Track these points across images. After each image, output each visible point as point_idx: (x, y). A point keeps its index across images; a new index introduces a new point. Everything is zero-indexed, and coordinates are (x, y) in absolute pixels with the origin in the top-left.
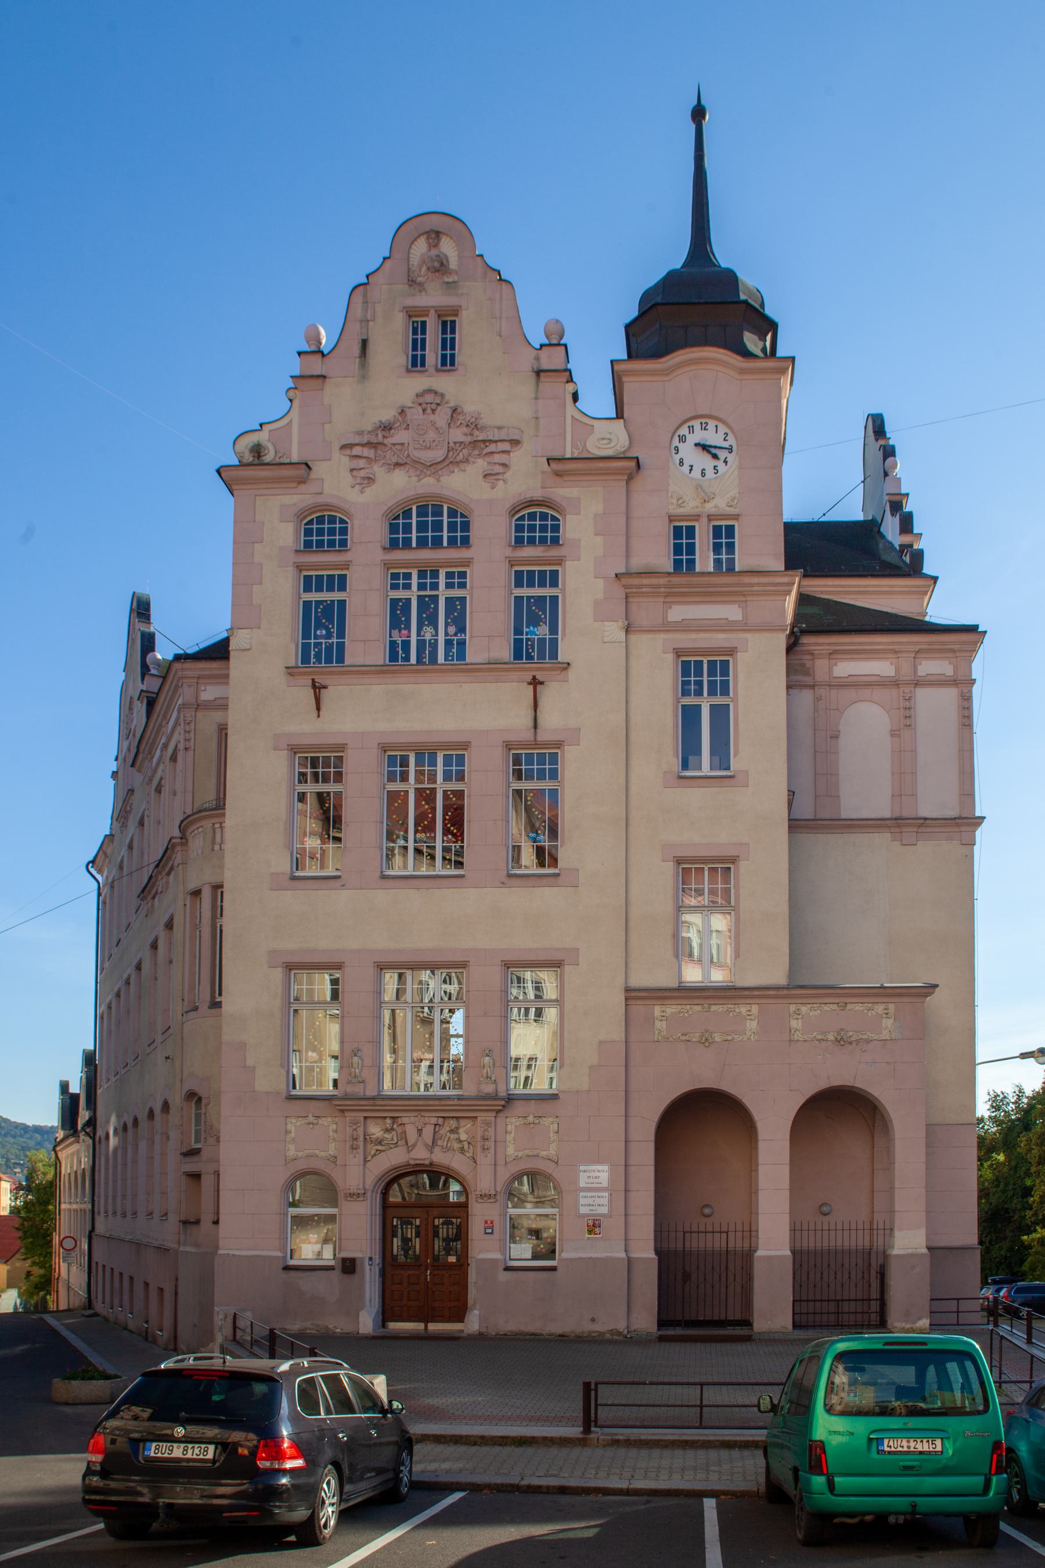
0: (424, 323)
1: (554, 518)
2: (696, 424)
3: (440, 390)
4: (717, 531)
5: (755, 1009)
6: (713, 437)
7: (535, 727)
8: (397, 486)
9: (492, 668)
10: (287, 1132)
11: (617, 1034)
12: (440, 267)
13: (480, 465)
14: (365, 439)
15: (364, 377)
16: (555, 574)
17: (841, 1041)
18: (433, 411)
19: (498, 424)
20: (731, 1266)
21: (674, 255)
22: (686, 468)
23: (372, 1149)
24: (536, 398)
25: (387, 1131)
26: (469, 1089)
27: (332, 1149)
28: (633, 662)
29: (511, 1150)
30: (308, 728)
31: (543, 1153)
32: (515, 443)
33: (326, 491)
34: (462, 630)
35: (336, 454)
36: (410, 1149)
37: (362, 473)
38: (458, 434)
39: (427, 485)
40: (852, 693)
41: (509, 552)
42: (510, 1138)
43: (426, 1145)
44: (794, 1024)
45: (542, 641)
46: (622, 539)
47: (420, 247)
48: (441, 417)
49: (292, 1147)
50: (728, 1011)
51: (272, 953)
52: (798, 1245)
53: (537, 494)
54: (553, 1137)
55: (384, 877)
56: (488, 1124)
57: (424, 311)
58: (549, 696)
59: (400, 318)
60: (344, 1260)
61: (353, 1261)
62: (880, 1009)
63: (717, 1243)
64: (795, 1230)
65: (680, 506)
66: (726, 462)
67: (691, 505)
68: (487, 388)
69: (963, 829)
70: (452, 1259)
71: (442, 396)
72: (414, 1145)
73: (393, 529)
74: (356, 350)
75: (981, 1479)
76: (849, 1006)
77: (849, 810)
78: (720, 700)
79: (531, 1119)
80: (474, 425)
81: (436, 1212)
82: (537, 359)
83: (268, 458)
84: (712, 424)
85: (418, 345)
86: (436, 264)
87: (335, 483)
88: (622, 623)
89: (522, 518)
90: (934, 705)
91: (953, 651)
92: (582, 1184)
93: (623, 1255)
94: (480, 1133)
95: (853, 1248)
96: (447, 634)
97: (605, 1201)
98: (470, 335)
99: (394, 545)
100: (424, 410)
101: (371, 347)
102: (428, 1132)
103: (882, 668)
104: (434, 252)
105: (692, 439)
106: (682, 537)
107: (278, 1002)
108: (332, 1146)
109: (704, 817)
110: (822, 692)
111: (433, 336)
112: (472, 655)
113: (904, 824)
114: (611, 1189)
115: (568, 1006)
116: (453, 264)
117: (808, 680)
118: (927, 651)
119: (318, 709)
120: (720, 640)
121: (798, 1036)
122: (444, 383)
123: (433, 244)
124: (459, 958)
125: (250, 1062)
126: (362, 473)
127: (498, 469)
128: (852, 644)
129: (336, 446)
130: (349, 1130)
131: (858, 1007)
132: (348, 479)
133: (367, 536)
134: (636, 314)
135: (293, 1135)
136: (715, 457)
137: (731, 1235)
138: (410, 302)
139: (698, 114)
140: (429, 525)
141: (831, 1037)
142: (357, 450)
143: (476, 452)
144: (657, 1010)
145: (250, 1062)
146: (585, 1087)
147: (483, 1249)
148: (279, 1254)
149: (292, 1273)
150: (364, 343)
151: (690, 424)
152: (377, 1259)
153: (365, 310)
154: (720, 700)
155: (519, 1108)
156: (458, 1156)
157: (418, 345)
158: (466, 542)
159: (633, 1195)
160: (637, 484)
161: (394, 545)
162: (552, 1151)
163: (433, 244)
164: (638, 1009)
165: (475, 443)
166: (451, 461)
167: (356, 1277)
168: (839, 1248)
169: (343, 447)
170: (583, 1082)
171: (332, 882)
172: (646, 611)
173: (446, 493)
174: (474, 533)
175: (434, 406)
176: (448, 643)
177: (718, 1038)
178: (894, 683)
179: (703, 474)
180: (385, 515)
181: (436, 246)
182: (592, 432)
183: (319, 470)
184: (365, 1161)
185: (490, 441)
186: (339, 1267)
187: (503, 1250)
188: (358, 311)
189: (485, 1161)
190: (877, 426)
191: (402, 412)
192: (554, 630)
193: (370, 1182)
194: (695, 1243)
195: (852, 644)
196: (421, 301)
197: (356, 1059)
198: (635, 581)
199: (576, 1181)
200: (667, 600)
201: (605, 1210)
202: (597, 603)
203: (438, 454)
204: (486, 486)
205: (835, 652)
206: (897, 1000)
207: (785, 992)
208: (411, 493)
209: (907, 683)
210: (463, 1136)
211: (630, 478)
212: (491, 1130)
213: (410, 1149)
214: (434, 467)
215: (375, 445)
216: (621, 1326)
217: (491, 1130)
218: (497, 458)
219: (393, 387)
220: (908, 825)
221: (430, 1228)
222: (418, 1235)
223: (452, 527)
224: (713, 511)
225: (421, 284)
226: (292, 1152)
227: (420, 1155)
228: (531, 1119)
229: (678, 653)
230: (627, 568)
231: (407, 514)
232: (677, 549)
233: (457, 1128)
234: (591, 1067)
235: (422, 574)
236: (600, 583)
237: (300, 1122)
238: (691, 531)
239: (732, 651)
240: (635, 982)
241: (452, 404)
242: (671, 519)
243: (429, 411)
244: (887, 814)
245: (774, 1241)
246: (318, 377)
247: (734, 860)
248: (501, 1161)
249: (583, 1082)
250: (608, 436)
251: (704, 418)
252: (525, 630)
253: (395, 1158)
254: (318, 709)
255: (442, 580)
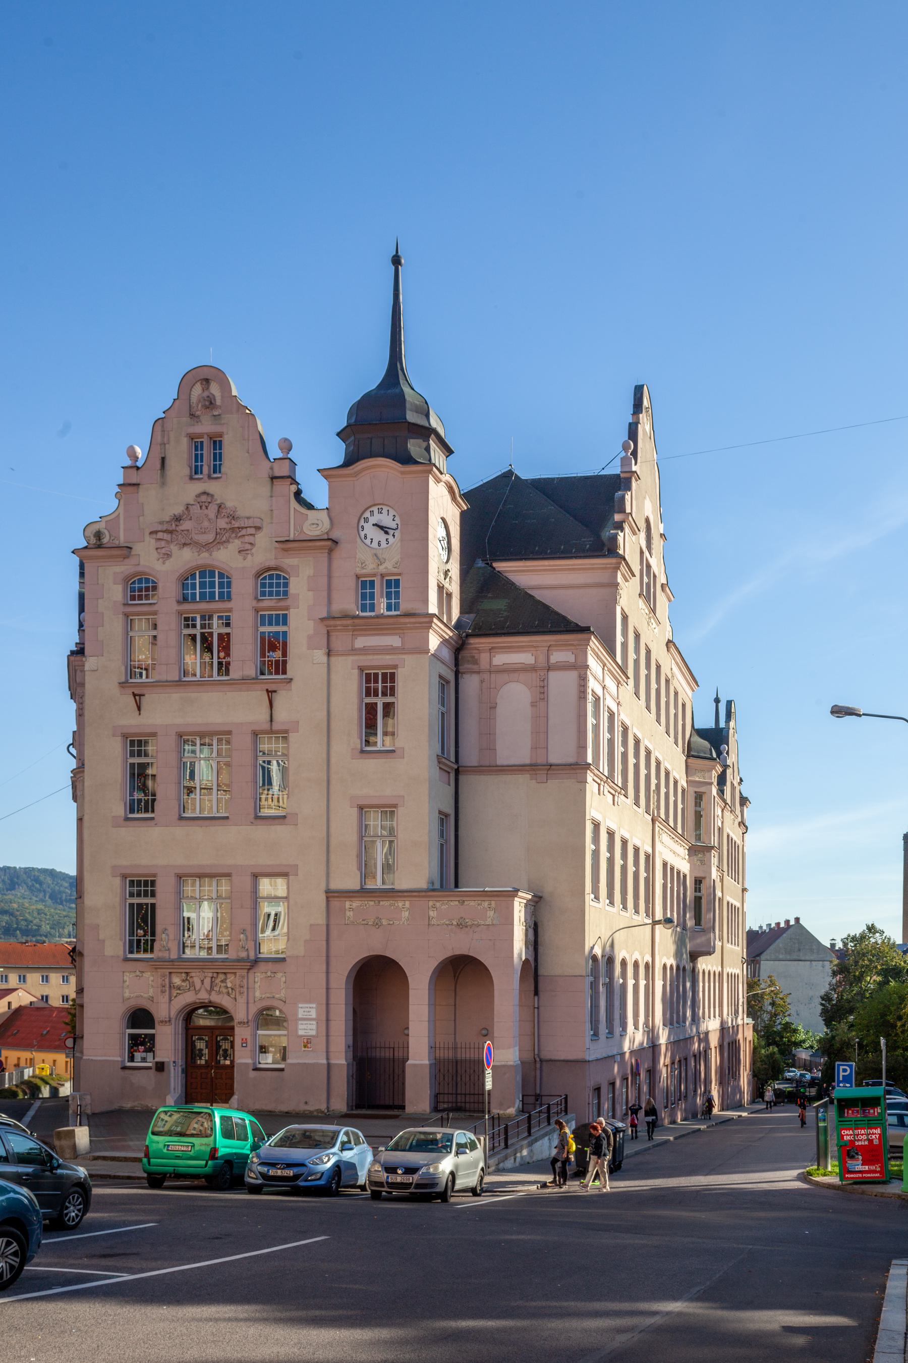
0: (202, 443)
1: (285, 578)
2: (375, 509)
3: (211, 492)
4: (389, 583)
5: (407, 904)
6: (387, 521)
7: (271, 721)
8: (185, 558)
9: (245, 681)
10: (124, 982)
11: (321, 920)
12: (210, 403)
13: (236, 544)
14: (165, 527)
15: (163, 484)
16: (285, 617)
17: (461, 925)
18: (207, 508)
19: (248, 515)
20: (396, 1071)
21: (372, 376)
22: (368, 541)
23: (175, 992)
24: (271, 497)
25: (183, 981)
26: (232, 954)
27: (151, 992)
28: (333, 676)
29: (258, 994)
30: (132, 722)
31: (277, 996)
32: (258, 528)
33: (142, 562)
34: (228, 654)
35: (147, 538)
36: (197, 992)
37: (163, 551)
38: (222, 523)
39: (204, 558)
40: (505, 677)
41: (254, 603)
42: (257, 985)
43: (206, 990)
44: (431, 913)
45: (277, 662)
46: (325, 594)
47: (197, 390)
48: (212, 511)
49: (127, 991)
50: (391, 905)
51: (114, 867)
52: (437, 1055)
53: (272, 563)
54: (283, 985)
55: (181, 818)
56: (243, 977)
57: (201, 436)
58: (278, 700)
59: (185, 441)
60: (157, 1063)
61: (162, 1064)
62: (486, 904)
63: (388, 1054)
64: (432, 1048)
65: (363, 568)
66: (394, 536)
67: (370, 567)
68: (241, 490)
69: (578, 771)
70: (228, 1062)
71: (212, 496)
72: (199, 990)
73: (184, 586)
74: (158, 466)
75: (204, 1162)
76: (466, 903)
77: (503, 759)
78: (389, 699)
79: (269, 974)
80: (233, 517)
81: (217, 1032)
82: (272, 468)
83: (105, 540)
84: (385, 509)
85: (198, 458)
86: (207, 403)
87: (147, 557)
88: (324, 650)
89: (265, 578)
90: (561, 683)
91: (573, 645)
92: (300, 1016)
93: (325, 1062)
94: (238, 983)
95: (459, 1058)
96: (219, 658)
97: (314, 1027)
98: (231, 451)
99: (185, 599)
100: (201, 507)
101: (167, 462)
102: (207, 981)
103: (526, 658)
104: (206, 394)
105: (373, 520)
106: (365, 586)
107: (118, 899)
108: (151, 990)
109: (373, 778)
110: (486, 676)
111: (207, 452)
112: (235, 673)
113: (541, 769)
114: (317, 1020)
115: (291, 902)
116: (218, 402)
117: (475, 667)
118: (556, 645)
119: (139, 708)
120: (387, 659)
121: (434, 922)
122: (212, 487)
123: (204, 392)
124: (226, 871)
125: (101, 937)
126: (163, 551)
127: (248, 546)
128: (504, 642)
129: (147, 533)
130: (160, 981)
131: (472, 903)
132: (155, 554)
133: (168, 590)
134: (345, 424)
135: (127, 983)
136: (386, 533)
137: (396, 1050)
138: (192, 430)
139: (396, 261)
140: (205, 584)
141: (455, 923)
142: (160, 535)
143: (234, 535)
144: (347, 904)
145: (101, 937)
146: (302, 953)
147: (242, 1057)
148: (119, 1059)
149: (127, 1072)
150: (163, 460)
151: (371, 509)
152: (180, 1062)
153: (163, 436)
154: (389, 699)
155: (262, 966)
156: (226, 997)
157: (198, 458)
158: (229, 598)
159: (332, 1023)
160: (336, 554)
161: (185, 599)
162: (282, 995)
163: (204, 392)
164: (335, 903)
165: (233, 530)
166: (219, 541)
167: (165, 1074)
168: (472, 1059)
169: (151, 533)
170: (301, 951)
171: (149, 822)
172: (340, 641)
173: (215, 563)
174: (234, 590)
175: (206, 504)
176: (220, 664)
177: (384, 922)
178: (532, 669)
179: (379, 544)
180: (179, 579)
181: (208, 388)
182: (307, 519)
183: (138, 548)
184: (170, 1000)
185: (242, 528)
186: (154, 1068)
187: (253, 1057)
188: (158, 438)
189: (242, 1000)
190: (638, 391)
191: (188, 507)
192: (285, 654)
193: (173, 1013)
194: (378, 1054)
195: (504, 642)
196: (198, 429)
197: (164, 936)
198: (332, 622)
199: (296, 1014)
200: (355, 633)
201: (314, 1033)
202: (310, 638)
203: (210, 537)
204: (240, 558)
205: (493, 648)
206: (496, 899)
207: (423, 894)
208: (194, 564)
209: (542, 669)
210: (229, 985)
211: (330, 551)
212: (245, 981)
213: (197, 992)
214: (207, 547)
215: (172, 530)
216: (323, 1107)
217: (245, 981)
218: (247, 539)
219: (182, 491)
220: (540, 770)
221: (214, 1042)
222: (207, 1047)
223: (221, 585)
224: (384, 571)
225: (198, 417)
226: (127, 995)
227: (203, 996)
228: (269, 974)
229: (361, 669)
230: (328, 612)
231: (193, 576)
232: (364, 596)
233: (226, 979)
234: (305, 941)
235: (203, 618)
236: (311, 623)
237: (133, 975)
238: (372, 583)
239: (395, 667)
240: (334, 886)
241: (219, 502)
242: (358, 577)
243: (204, 507)
244: (527, 761)
245: (419, 1054)
246: (134, 485)
247: (395, 806)
248: (251, 1001)
249: (301, 951)
250: (316, 522)
251: (380, 506)
252: (267, 654)
253: (188, 998)
254: (139, 708)
255: (215, 621)
